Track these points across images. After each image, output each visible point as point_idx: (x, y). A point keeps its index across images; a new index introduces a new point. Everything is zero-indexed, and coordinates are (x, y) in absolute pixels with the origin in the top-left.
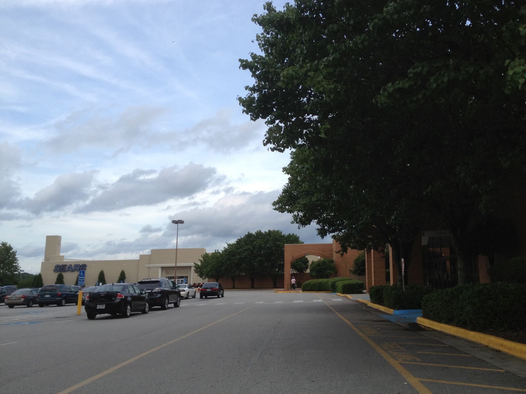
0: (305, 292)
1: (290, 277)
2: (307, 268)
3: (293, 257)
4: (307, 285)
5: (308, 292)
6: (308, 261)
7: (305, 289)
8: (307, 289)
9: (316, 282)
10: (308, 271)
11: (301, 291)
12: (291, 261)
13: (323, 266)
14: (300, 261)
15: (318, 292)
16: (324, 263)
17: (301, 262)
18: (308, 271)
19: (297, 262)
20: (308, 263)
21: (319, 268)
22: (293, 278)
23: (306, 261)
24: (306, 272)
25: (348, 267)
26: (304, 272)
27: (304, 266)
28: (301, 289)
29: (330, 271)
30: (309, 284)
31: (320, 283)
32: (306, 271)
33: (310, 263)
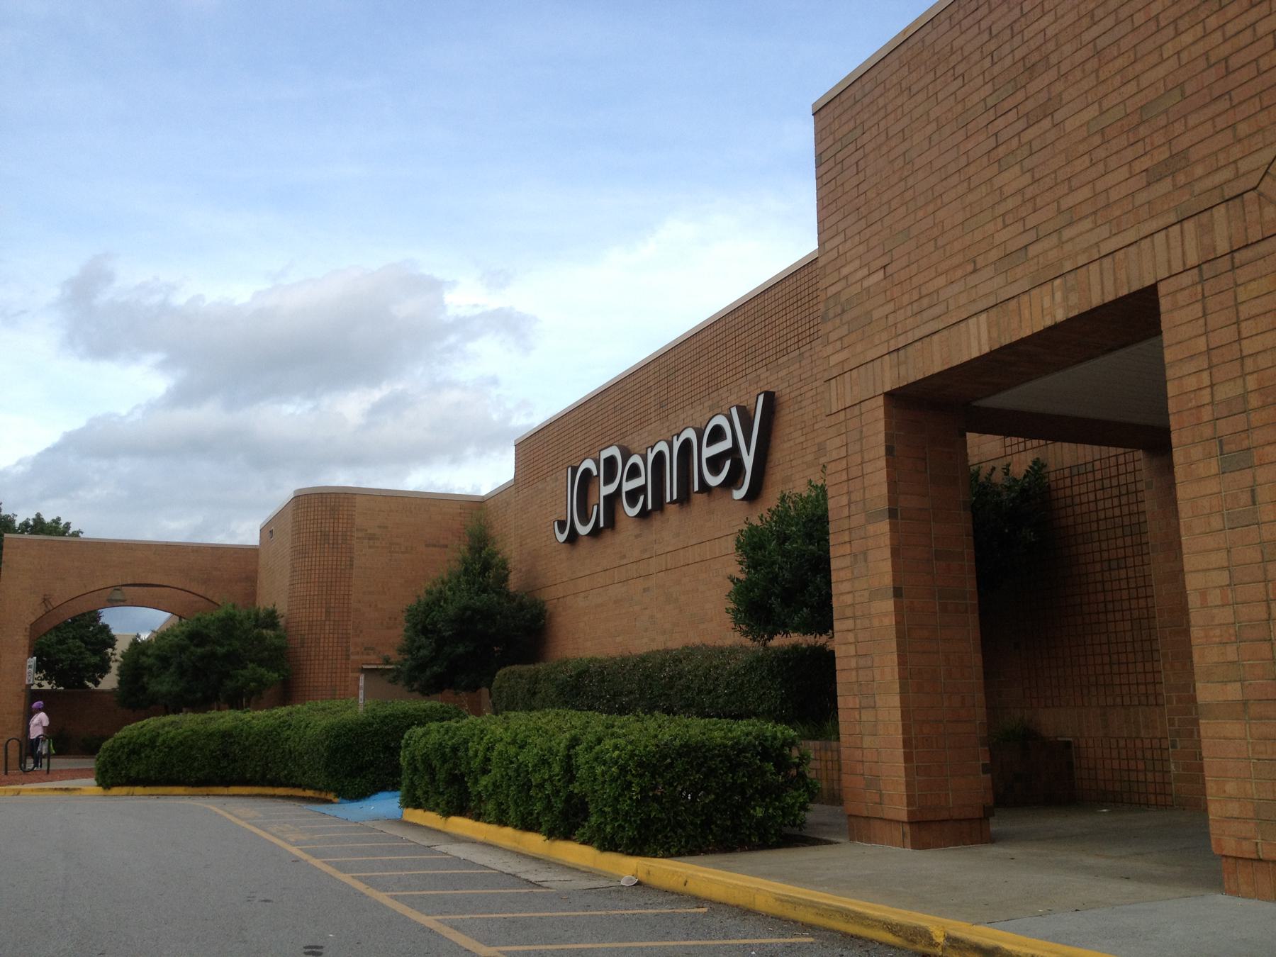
0: (115, 790)
1: (20, 706)
2: (104, 668)
3: (45, 601)
4: (135, 750)
5: (139, 790)
6: (110, 641)
7: (111, 777)
8: (133, 774)
9: (194, 732)
10: (110, 682)
11: (89, 785)
12: (33, 619)
13: (222, 645)
14: (74, 638)
15: (204, 790)
16: (196, 637)
17: (79, 643)
18: (110, 682)
19: (61, 642)
20: (112, 646)
21: (199, 650)
22: (39, 710)
23: (105, 639)
24: (101, 687)
25: (352, 649)
26: (90, 685)
27: (95, 660)
28: (90, 763)
29: (262, 670)
30: (152, 743)
31: (226, 735)
32: (97, 683)
33: (122, 646)
